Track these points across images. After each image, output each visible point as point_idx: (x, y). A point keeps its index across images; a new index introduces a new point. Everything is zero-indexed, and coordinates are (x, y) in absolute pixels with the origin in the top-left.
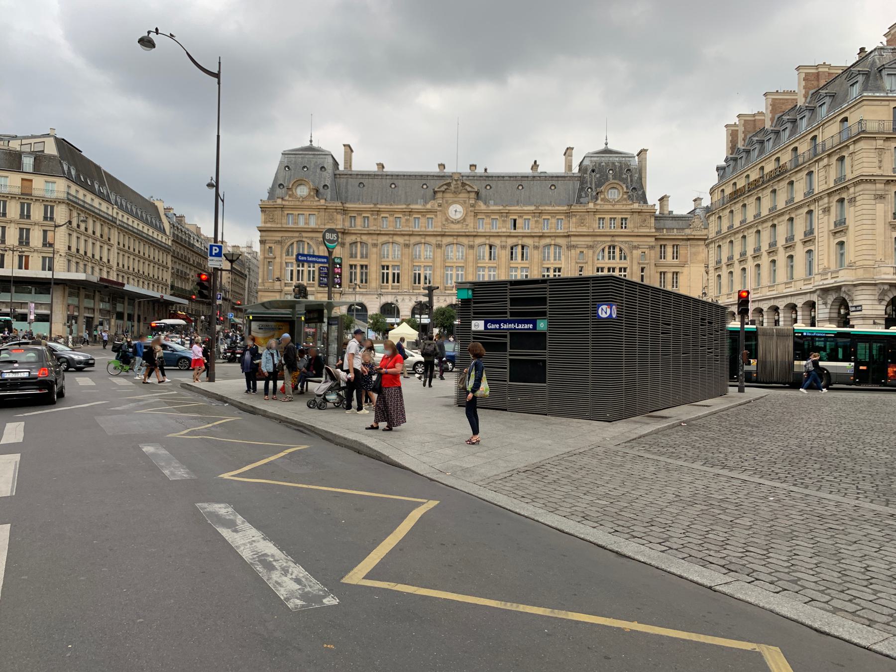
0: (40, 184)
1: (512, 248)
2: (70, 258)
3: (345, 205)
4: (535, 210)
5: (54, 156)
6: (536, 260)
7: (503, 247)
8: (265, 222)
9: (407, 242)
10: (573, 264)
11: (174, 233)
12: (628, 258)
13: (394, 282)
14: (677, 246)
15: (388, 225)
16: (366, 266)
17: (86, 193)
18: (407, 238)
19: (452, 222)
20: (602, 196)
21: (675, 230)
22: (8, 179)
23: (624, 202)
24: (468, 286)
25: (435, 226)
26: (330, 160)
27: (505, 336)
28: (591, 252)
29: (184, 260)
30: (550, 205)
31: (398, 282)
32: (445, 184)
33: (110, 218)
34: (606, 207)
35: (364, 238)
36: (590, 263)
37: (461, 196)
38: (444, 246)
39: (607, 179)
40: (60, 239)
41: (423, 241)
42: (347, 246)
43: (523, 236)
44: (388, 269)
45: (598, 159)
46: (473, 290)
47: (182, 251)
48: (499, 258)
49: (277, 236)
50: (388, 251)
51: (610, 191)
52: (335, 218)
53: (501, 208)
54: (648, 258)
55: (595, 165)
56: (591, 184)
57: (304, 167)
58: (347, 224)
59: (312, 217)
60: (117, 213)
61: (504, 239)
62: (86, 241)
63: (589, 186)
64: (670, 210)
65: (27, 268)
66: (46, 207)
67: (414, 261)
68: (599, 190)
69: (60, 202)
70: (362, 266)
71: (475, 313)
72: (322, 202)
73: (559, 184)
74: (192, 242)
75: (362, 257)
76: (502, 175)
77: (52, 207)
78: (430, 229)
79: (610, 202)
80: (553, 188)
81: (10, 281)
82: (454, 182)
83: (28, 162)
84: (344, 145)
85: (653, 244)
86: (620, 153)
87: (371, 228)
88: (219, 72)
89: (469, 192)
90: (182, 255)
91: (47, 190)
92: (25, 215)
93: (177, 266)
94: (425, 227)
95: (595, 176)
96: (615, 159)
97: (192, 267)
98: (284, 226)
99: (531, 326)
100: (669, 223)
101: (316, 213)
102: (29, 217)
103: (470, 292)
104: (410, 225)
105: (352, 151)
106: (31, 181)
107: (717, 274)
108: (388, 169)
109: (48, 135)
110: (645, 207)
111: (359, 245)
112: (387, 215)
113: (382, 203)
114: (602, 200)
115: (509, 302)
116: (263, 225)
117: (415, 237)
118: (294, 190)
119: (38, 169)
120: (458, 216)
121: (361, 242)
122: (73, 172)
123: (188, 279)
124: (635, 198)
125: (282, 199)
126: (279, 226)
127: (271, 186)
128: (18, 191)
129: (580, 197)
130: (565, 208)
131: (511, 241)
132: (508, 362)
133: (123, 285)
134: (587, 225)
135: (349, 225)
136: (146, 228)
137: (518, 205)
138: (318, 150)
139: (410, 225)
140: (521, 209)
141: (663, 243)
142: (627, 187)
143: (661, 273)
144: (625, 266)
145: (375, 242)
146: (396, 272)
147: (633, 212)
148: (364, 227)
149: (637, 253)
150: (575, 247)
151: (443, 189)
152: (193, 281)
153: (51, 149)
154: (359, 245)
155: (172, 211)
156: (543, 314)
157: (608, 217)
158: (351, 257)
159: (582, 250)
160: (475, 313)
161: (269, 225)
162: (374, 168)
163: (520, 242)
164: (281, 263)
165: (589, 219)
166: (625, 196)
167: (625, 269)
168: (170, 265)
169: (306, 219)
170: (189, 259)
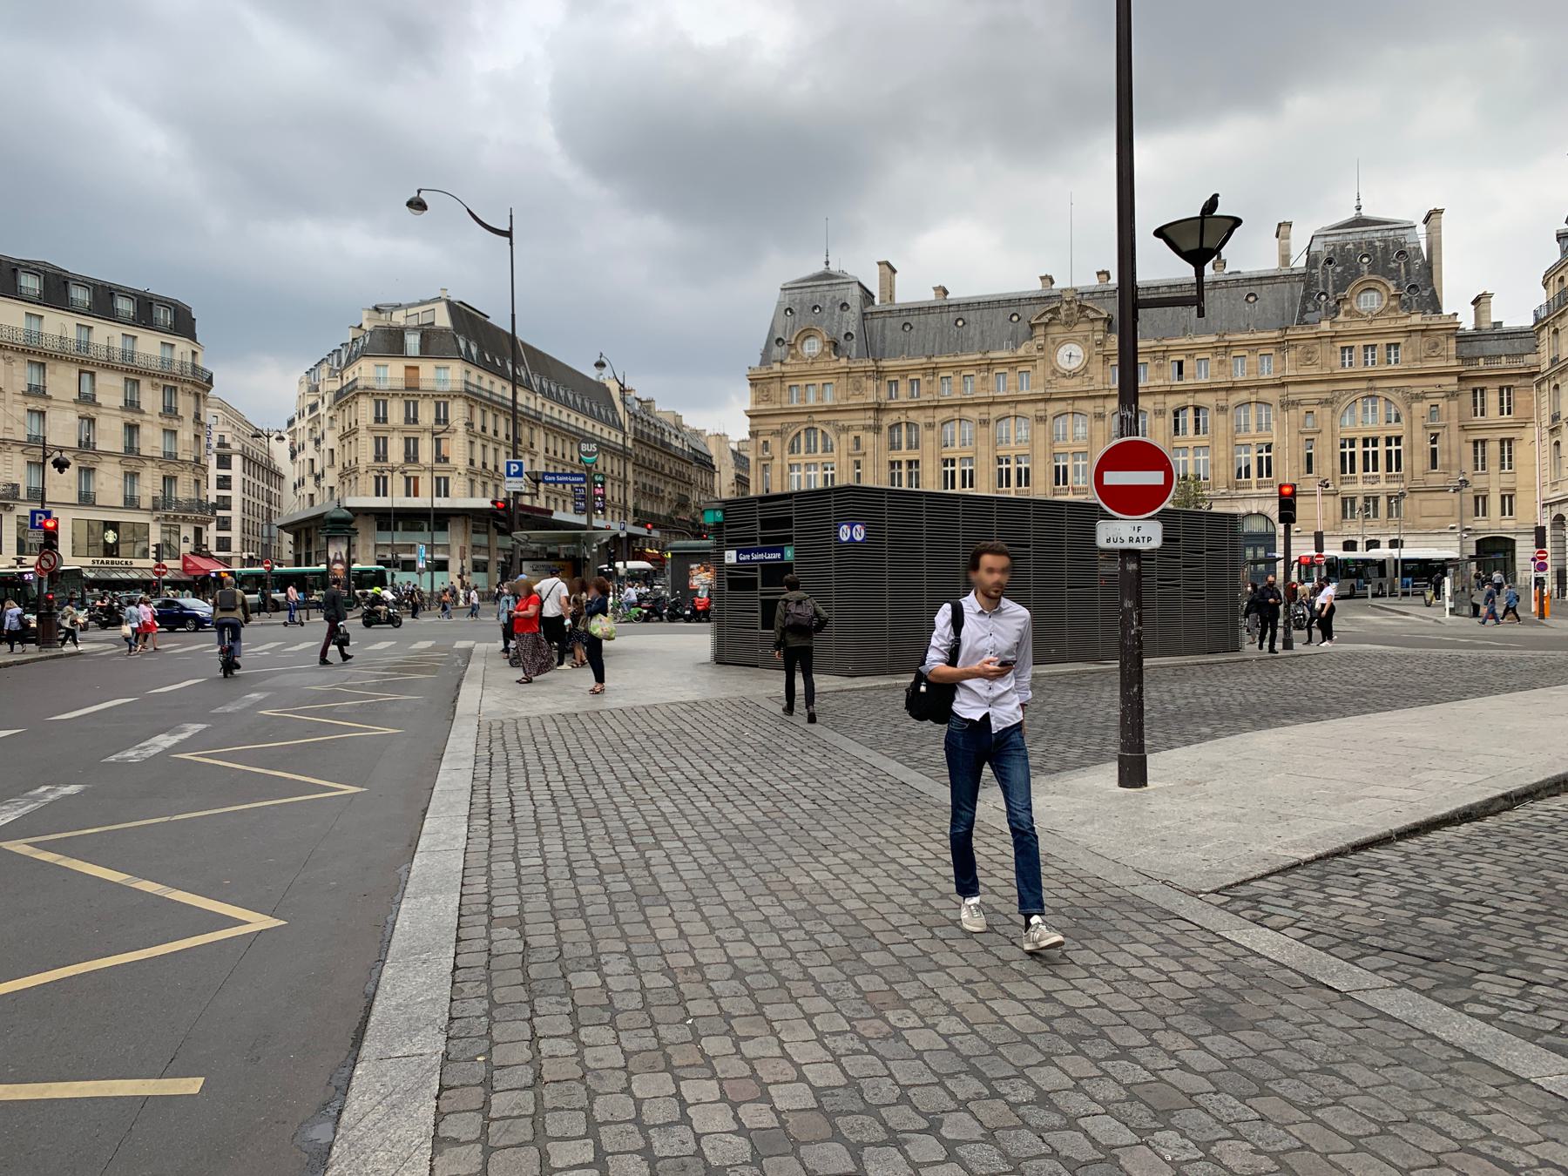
0: (430, 373)
1: (1176, 414)
2: (473, 477)
3: (879, 364)
4: (1218, 341)
5: (446, 329)
6: (1221, 432)
7: (1160, 413)
8: (757, 403)
9: (985, 417)
10: (1294, 435)
11: (635, 429)
12: (1403, 419)
13: (1019, 484)
14: (1509, 388)
15: (951, 390)
16: (917, 462)
17: (493, 378)
18: (984, 409)
19: (1064, 376)
20: (1347, 307)
21: (1504, 358)
22: (449, 372)
23: (1393, 315)
24: (717, 505)
25: (1034, 383)
26: (856, 290)
27: (755, 570)
28: (1328, 411)
29: (654, 469)
30: (1247, 330)
31: (1027, 484)
32: (1049, 311)
33: (532, 413)
34: (1355, 326)
35: (913, 415)
36: (1327, 432)
37: (1077, 328)
38: (1050, 419)
39: (1358, 274)
40: (457, 448)
41: (1012, 412)
42: (885, 430)
43: (1196, 391)
44: (953, 465)
45: (1340, 237)
46: (724, 511)
47: (648, 455)
48: (1151, 432)
49: (776, 423)
50: (1065, 427)
51: (1362, 296)
52: (864, 385)
53: (1153, 343)
54: (1445, 417)
55: (1334, 250)
56: (1325, 286)
57: (815, 307)
58: (884, 395)
59: (828, 387)
60: (543, 405)
61: (1160, 398)
62: (496, 450)
63: (1322, 290)
64: (1493, 320)
65: (416, 495)
66: (438, 404)
67: (1057, 443)
68: (1340, 295)
69: (455, 395)
70: (910, 463)
71: (728, 541)
72: (843, 361)
73: (1264, 292)
74: (667, 440)
75: (910, 447)
76: (1155, 284)
77: (446, 404)
78: (1025, 391)
79: (1363, 316)
80: (1251, 299)
81: (389, 515)
82: (1065, 306)
83: (413, 342)
84: (879, 263)
85: (1455, 388)
86: (1386, 223)
87: (922, 398)
88: (511, 228)
89: (1092, 320)
90: (650, 461)
91: (438, 381)
92: (412, 419)
93: (643, 479)
94: (1016, 388)
95: (1333, 271)
96: (1373, 234)
97: (668, 479)
98: (785, 406)
99: (778, 555)
100: (1492, 347)
101: (834, 381)
102: (416, 421)
103: (719, 515)
104: (990, 386)
105: (894, 271)
106: (417, 368)
107: (1554, 441)
108: (955, 294)
109: (439, 299)
110: (1435, 320)
111: (904, 427)
112: (951, 374)
113: (941, 354)
114: (1347, 313)
115: (758, 525)
116: (754, 407)
117: (998, 407)
118: (799, 347)
119: (426, 352)
120: (1075, 364)
121: (907, 423)
122: (474, 350)
123: (663, 498)
124: (1415, 305)
125: (782, 362)
126: (778, 406)
127: (763, 347)
128: (401, 385)
129: (1304, 311)
130: (1276, 334)
131: (1173, 402)
132: (759, 604)
133: (551, 513)
134: (1319, 361)
135: (887, 396)
136: (590, 423)
137: (1184, 335)
138: (837, 277)
139: (990, 386)
140: (1190, 342)
141: (1477, 385)
142: (1398, 286)
143: (1475, 443)
144: (1397, 433)
145: (931, 420)
146: (968, 468)
147: (1410, 332)
148: (912, 397)
149: (1420, 408)
150: (1296, 404)
151: (1045, 319)
152: (671, 501)
153: (443, 320)
154: (904, 427)
155: (633, 394)
156: (788, 539)
157: (1359, 344)
158: (892, 448)
159: (1310, 408)
160: (728, 541)
161: (762, 407)
162: (929, 296)
163: (1190, 402)
164: (782, 466)
165: (1321, 350)
166: (1393, 303)
167: (1398, 440)
168: (630, 477)
169: (818, 392)
170: (663, 466)
